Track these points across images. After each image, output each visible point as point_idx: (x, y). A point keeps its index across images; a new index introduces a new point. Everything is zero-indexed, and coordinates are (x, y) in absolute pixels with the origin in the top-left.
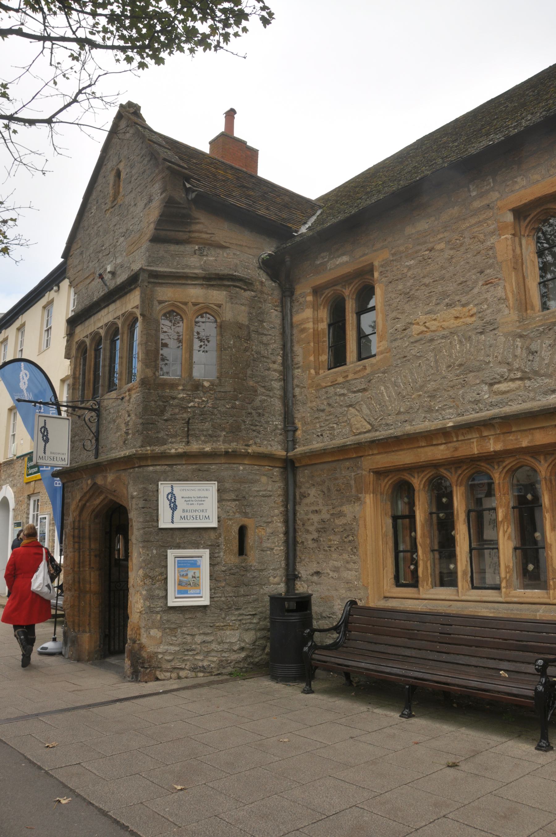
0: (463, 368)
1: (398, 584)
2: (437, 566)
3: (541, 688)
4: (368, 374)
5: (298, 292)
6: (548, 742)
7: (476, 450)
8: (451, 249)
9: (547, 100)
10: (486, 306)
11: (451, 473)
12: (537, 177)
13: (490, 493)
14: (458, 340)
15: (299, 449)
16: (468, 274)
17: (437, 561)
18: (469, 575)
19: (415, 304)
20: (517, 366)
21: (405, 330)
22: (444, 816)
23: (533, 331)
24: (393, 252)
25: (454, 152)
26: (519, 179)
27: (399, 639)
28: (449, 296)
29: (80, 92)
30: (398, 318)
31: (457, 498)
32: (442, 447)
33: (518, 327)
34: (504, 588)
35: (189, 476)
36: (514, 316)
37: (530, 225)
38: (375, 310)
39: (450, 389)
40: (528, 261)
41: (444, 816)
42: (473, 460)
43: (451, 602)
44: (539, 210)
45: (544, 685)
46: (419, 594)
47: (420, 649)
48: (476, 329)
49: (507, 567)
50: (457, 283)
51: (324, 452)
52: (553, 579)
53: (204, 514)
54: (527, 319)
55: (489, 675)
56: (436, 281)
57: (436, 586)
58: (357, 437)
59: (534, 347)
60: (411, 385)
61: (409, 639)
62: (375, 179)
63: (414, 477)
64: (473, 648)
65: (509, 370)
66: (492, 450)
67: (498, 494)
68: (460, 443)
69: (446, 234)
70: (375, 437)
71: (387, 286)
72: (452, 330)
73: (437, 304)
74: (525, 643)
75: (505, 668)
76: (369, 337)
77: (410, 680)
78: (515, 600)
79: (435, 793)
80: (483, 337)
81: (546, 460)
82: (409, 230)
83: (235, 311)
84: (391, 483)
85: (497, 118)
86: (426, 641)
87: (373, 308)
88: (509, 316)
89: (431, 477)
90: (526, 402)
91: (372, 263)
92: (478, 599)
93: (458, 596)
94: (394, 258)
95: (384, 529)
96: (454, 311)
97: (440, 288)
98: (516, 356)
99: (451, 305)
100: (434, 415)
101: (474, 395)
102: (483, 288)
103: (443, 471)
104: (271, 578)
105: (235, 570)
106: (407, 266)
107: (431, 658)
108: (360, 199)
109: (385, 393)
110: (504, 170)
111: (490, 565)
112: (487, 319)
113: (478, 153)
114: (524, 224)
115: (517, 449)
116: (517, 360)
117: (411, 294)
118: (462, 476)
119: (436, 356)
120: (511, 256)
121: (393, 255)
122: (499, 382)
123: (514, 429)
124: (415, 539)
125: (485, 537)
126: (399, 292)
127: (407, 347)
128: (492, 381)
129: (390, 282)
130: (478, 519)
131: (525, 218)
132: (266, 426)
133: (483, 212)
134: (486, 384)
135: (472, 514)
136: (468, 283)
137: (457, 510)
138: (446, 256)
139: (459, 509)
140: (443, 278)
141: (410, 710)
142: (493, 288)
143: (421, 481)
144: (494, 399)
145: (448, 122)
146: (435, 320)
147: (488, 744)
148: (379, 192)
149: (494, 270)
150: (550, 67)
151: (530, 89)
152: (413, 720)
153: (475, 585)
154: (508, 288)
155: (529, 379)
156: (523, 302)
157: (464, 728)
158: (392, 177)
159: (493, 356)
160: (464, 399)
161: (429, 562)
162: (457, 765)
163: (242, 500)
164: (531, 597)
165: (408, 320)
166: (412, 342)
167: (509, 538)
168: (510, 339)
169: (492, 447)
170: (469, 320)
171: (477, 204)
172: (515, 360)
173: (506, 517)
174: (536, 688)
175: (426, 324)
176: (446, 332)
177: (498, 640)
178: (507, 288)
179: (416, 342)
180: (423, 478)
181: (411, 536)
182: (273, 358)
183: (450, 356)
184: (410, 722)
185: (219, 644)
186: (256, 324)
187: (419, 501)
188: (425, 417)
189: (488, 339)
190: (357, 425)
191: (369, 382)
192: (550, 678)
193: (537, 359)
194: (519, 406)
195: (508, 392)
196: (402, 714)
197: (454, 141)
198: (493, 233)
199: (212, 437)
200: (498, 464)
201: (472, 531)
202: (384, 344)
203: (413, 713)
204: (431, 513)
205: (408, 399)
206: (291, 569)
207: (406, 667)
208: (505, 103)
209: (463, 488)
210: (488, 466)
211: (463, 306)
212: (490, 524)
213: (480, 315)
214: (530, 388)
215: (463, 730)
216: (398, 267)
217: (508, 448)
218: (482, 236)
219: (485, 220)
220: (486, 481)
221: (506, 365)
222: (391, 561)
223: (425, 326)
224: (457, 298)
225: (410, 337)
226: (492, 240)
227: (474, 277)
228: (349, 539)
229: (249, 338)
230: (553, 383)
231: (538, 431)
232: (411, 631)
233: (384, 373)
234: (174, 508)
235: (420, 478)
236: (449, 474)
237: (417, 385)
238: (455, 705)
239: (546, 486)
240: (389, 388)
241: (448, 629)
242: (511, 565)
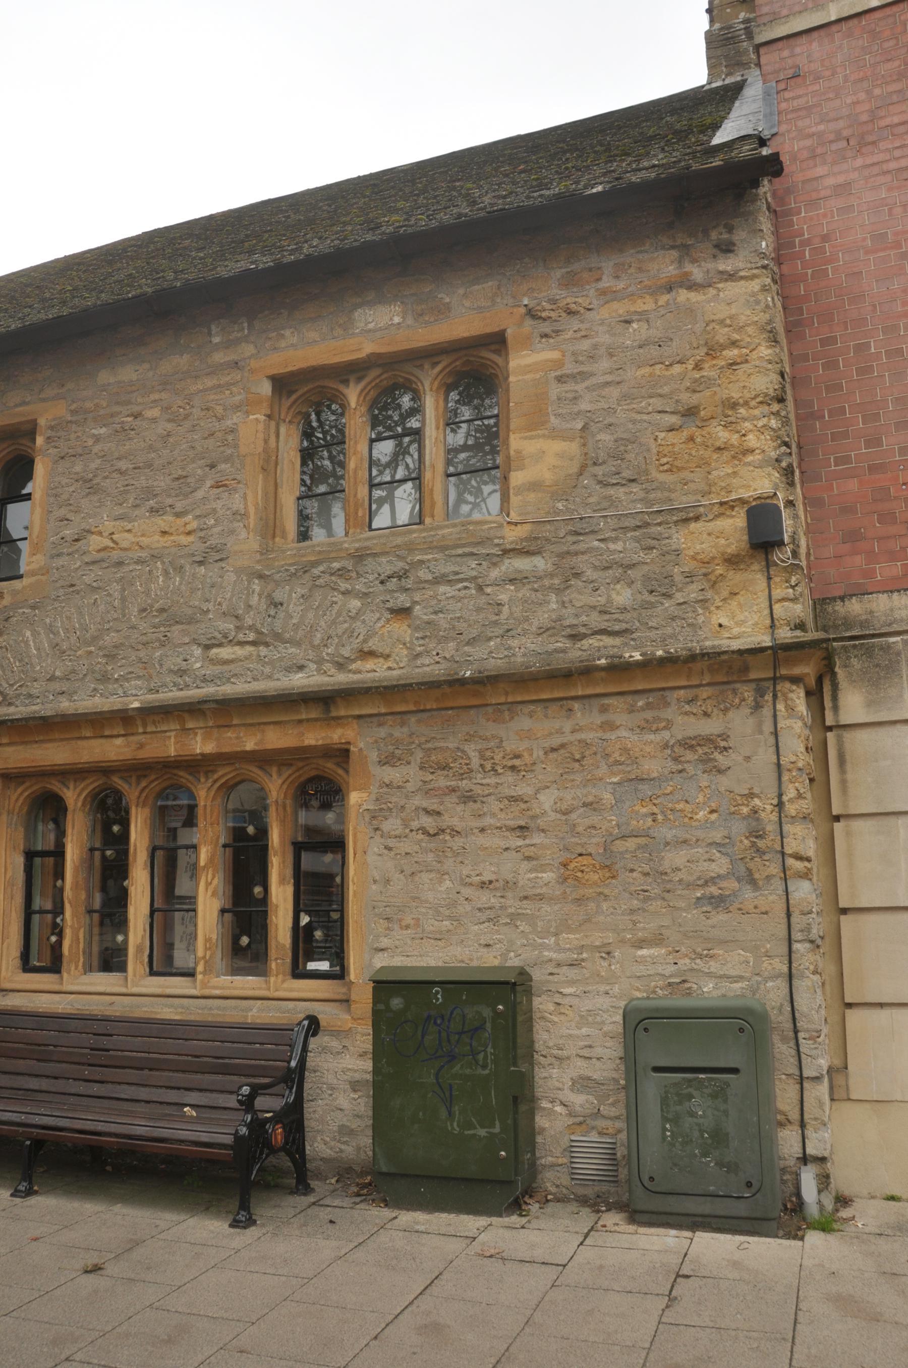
0: (165, 615)
1: (27, 966)
2: (96, 938)
3: (244, 1131)
4: (5, 607)
6: (249, 1213)
7: (173, 749)
8: (169, 421)
9: (345, 224)
10: (212, 522)
11: (130, 784)
12: (313, 335)
13: (190, 821)
14: (163, 569)
16: (191, 466)
17: (96, 930)
18: (147, 952)
19: (99, 501)
20: (250, 623)
21: (77, 540)
22: (67, 1359)
23: (280, 572)
24: (73, 407)
25: (195, 266)
26: (287, 333)
27: (21, 1061)
28: (156, 495)
30: (67, 520)
31: (136, 826)
32: (119, 741)
33: (258, 562)
34: (201, 973)
36: (254, 543)
37: (295, 407)
38: (30, 499)
39: (140, 647)
40: (285, 462)
41: (67, 1359)
42: (168, 766)
43: (114, 998)
44: (310, 386)
45: (249, 1126)
46: (62, 984)
47: (56, 1078)
48: (193, 555)
49: (207, 940)
50: (171, 477)
52: (276, 959)
54: (272, 551)
55: (167, 1115)
56: (139, 468)
57: (91, 971)
59: (278, 596)
60: (78, 633)
61: (38, 1060)
62: (62, 280)
63: (68, 788)
64: (146, 1072)
65: (237, 627)
66: (198, 751)
67: (201, 823)
68: (148, 736)
69: (164, 395)
70: (5, 715)
71: (56, 462)
72: (155, 553)
73: (136, 506)
74: (227, 1061)
75: (192, 1103)
76: (18, 543)
77: (33, 1130)
78: (217, 992)
79: (57, 1321)
80: (202, 570)
81: (280, 774)
82: (105, 377)
84: (28, 796)
85: (271, 231)
86: (67, 1062)
87: (28, 497)
88: (245, 543)
89: (97, 790)
90: (258, 680)
91: (36, 420)
92: (158, 991)
93: (127, 987)
94: (74, 419)
95: (9, 874)
96: (165, 521)
97: (142, 482)
98: (250, 606)
99: (158, 512)
100: (111, 686)
101: (179, 660)
102: (211, 493)
103: (117, 781)
106: (94, 435)
107: (73, 1091)
108: (30, 307)
109: (31, 643)
110: (266, 312)
111: (182, 937)
112: (213, 542)
113: (230, 277)
114: (287, 403)
115: (237, 752)
116: (252, 613)
117: (94, 482)
118: (147, 790)
119: (124, 590)
120: (261, 449)
121: (74, 412)
122: (220, 645)
123: (235, 722)
124: (62, 890)
125: (178, 892)
126: (76, 477)
127: (77, 569)
128: (209, 642)
129: (62, 458)
130: (169, 862)
131: (290, 393)
133: (226, 372)
134: (199, 645)
135: (159, 854)
136: (189, 480)
137: (135, 845)
138: (160, 431)
139: (138, 845)
140: (149, 465)
141: (30, 1183)
142: (226, 494)
143: (79, 795)
144: (210, 670)
145: (197, 217)
146: (129, 531)
147: (156, 1226)
148: (64, 303)
149: (231, 467)
150: (359, 177)
151: (326, 200)
152: (33, 1200)
153: (155, 969)
154: (250, 498)
155: (267, 645)
156: (271, 523)
157: (119, 1205)
158: (91, 282)
159: (215, 602)
160: (161, 665)
161: (82, 931)
162: (100, 1269)
164: (242, 988)
165: (84, 526)
166: (87, 563)
167: (214, 894)
168: (245, 578)
169: (198, 747)
170: (184, 540)
171: (219, 357)
172: (248, 613)
173: (211, 860)
174: (237, 1131)
175: (114, 536)
176: (144, 554)
177: (186, 1058)
178: (249, 497)
179: (94, 563)
180: (83, 790)
181: (55, 886)
183: (147, 593)
184: (26, 1204)
187: (73, 828)
188: (95, 689)
189: (211, 574)
191: (6, 620)
192: (259, 1114)
193: (282, 615)
194: (246, 686)
196: (16, 1191)
197: (200, 249)
198: (237, 408)
200: (207, 774)
201: (156, 880)
202: (39, 561)
203: (36, 1188)
204: (92, 850)
205: (69, 656)
207: (28, 1110)
208: (287, 211)
209: (147, 811)
210: (190, 778)
211: (178, 515)
212: (186, 871)
213: (202, 534)
214: (266, 660)
215: (118, 1208)
216: (79, 434)
217: (224, 750)
218: (219, 410)
219: (228, 385)
220: (186, 802)
221: (234, 619)
222: (16, 928)
223: (112, 539)
224: (169, 501)
225: (85, 553)
226: (235, 418)
227: (199, 471)
230: (302, 654)
231: (272, 727)
232: (43, 1048)
233: (33, 608)
235: (78, 790)
236: (126, 786)
237: (88, 635)
238: (109, 1168)
239: (278, 814)
240: (39, 634)
241: (105, 1042)
242: (214, 937)
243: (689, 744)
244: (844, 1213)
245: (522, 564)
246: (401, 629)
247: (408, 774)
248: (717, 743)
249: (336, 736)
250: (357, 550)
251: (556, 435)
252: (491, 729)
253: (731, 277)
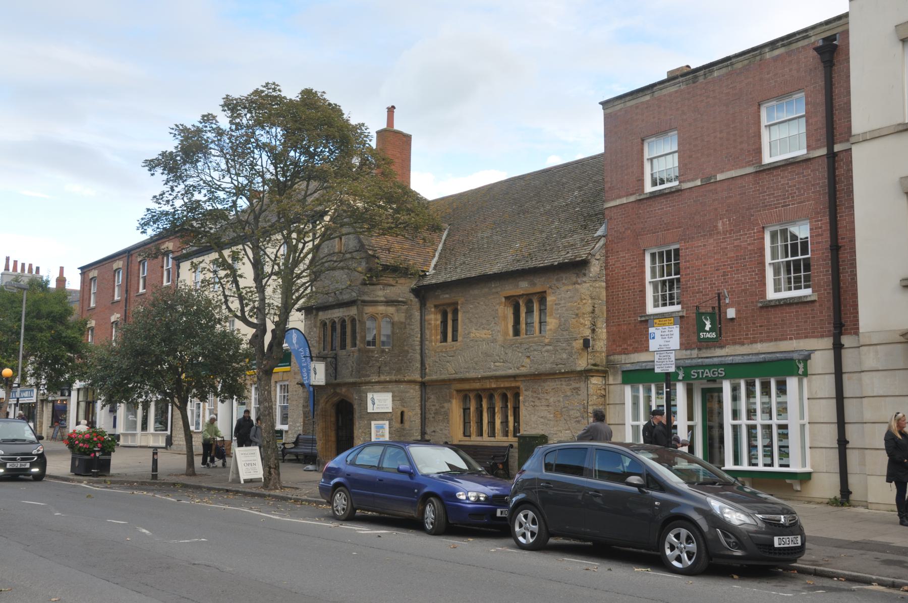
15: (427, 378)
51: (436, 381)
82: (471, 292)
83: (399, 317)
163: (402, 400)
171: (494, 290)
190: (450, 370)
199: (389, 373)
228: (446, 417)
229: (405, 328)
234: (374, 404)
243: (574, 389)
245: (549, 347)
246: (528, 360)
247: (529, 393)
248: (578, 389)
249: (517, 384)
251: (555, 318)
252: (543, 384)
253: (585, 282)
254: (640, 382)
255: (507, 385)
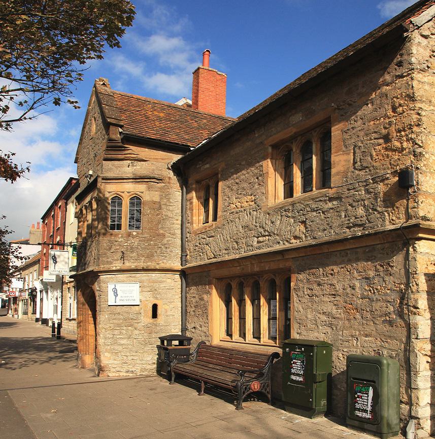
5: (190, 182)
15: (188, 265)
29: (35, 103)
35: (125, 280)
53: (132, 298)
58: (210, 260)
59: (273, 220)
82: (232, 153)
104: (173, 330)
105: (149, 325)
132: (170, 253)
163: (153, 291)
182: (176, 218)
185: (141, 360)
186: (165, 201)
195: (263, 242)
206: (183, 326)
209: (250, 289)
229: (160, 208)
244: (19, 259)
250: (292, 202)
254: (327, 401)
255: (273, 266)
